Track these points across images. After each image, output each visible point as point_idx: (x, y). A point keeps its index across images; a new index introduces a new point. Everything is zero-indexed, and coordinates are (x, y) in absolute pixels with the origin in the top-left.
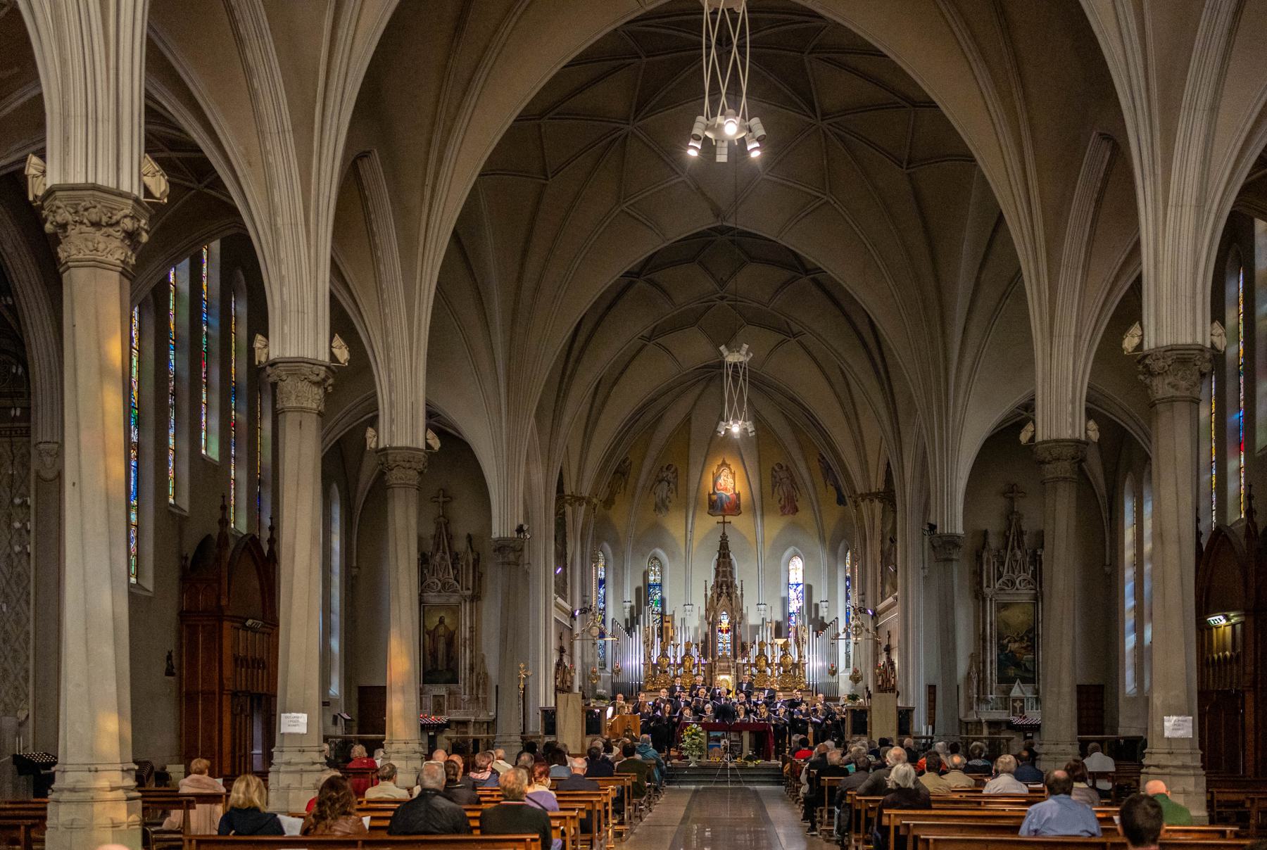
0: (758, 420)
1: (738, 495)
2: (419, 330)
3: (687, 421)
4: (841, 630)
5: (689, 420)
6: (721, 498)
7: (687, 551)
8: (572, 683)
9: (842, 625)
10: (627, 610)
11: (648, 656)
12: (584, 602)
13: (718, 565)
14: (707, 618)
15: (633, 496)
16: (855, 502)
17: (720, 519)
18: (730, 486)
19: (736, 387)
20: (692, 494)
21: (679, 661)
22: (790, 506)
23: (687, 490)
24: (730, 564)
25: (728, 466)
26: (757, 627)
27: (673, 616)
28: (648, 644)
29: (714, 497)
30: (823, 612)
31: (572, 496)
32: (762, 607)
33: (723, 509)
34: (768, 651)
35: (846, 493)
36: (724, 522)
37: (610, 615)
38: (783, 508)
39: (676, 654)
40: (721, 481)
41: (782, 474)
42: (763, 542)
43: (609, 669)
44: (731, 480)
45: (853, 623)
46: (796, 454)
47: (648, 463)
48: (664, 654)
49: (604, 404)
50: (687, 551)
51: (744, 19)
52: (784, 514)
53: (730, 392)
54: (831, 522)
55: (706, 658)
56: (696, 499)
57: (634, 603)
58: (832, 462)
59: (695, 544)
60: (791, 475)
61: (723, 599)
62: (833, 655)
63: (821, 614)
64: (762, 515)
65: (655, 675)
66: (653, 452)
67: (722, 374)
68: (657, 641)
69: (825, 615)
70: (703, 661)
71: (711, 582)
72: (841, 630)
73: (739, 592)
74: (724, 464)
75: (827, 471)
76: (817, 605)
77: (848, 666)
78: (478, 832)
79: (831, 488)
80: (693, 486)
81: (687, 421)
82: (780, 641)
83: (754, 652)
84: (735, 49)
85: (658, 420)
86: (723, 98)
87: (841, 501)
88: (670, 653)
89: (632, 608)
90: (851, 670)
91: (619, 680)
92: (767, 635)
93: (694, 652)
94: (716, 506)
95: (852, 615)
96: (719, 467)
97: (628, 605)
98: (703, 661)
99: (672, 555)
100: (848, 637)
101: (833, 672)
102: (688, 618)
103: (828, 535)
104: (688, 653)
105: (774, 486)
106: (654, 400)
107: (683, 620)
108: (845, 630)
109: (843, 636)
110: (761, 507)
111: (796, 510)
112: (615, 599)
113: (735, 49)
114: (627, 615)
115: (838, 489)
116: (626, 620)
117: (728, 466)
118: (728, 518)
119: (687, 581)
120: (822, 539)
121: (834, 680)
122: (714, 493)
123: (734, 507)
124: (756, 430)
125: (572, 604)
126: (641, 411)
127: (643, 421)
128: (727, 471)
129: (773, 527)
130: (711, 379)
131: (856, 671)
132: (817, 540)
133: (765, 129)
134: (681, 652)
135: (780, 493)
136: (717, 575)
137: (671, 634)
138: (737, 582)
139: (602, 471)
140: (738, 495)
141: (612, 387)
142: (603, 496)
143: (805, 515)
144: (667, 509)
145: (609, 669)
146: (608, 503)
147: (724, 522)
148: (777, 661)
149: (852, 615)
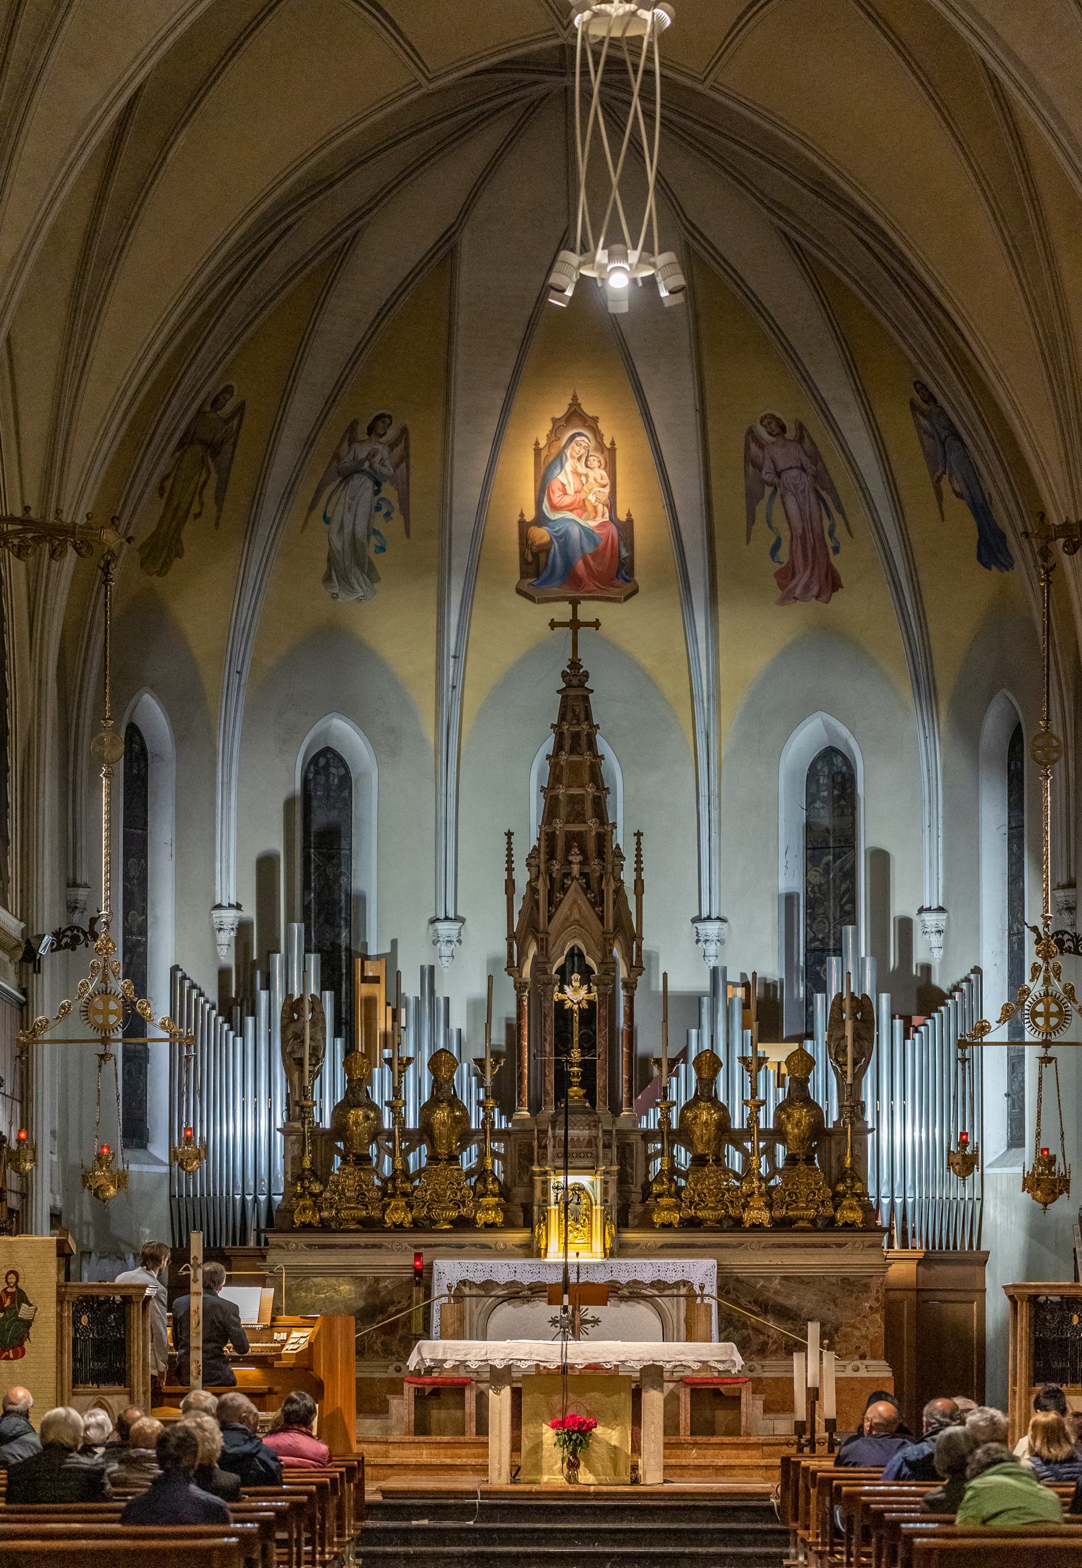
0: (698, 256)
1: (626, 529)
2: (236, 711)
3: (444, 255)
4: (991, 1011)
5: (453, 252)
6: (564, 538)
7: (445, 728)
8: (24, 1195)
9: (994, 997)
10: (227, 937)
11: (299, 1106)
12: (72, 907)
13: (556, 777)
14: (513, 967)
15: (250, 524)
16: (1045, 553)
17: (562, 611)
18: (597, 495)
19: (616, 124)
20: (462, 523)
21: (411, 1123)
22: (810, 573)
23: (445, 506)
24: (596, 776)
25: (591, 424)
26: (694, 1000)
27: (390, 959)
28: (300, 1063)
29: (541, 535)
30: (927, 948)
31: (26, 522)
32: (711, 929)
33: (571, 577)
34: (732, 1089)
35: (1006, 517)
36: (575, 624)
37: (165, 949)
38: (785, 576)
39: (403, 1094)
40: (565, 477)
41: (785, 455)
42: (715, 695)
43: (160, 1149)
44: (599, 474)
45: (1036, 988)
46: (834, 384)
47: (303, 406)
48: (355, 1095)
49: (143, 188)
50: (445, 728)
51: (650, 50)
52: (787, 598)
53: (596, 155)
54: (954, 628)
55: (508, 1110)
56: (477, 536)
57: (250, 912)
58: (961, 411)
59: (473, 700)
60: (816, 457)
61: (574, 902)
62: (965, 1098)
63: (920, 956)
64: (713, 599)
65: (321, 1173)
66: (319, 372)
67: (568, 91)
68: (334, 1049)
69: (936, 958)
70: (501, 1123)
71: (529, 838)
72: (991, 1011)
73: (628, 876)
74: (575, 415)
75: (944, 441)
76: (905, 925)
77: (1016, 1140)
78: (808, 1045)
79: (959, 510)
80: (466, 493)
81: (444, 255)
82: (777, 1053)
83: (682, 1087)
84: (636, 101)
85: (339, 252)
86: (616, 194)
87: (992, 550)
88: (380, 1091)
89: (243, 928)
90: (1028, 1152)
91: (196, 1188)
92: (728, 1036)
93: (468, 1089)
94: (547, 568)
95: (1031, 956)
96: (558, 426)
97: (229, 917)
98: (501, 1123)
99: (387, 742)
100: (1016, 1041)
101: (965, 1161)
102: (444, 968)
103: (945, 680)
104: (442, 1094)
105: (752, 499)
106: (321, 185)
107: (429, 975)
108: (1008, 1014)
109: (1000, 1033)
110: (709, 573)
111: (832, 583)
112: (181, 894)
113: (636, 101)
114: (227, 957)
115: (981, 511)
116: (223, 974)
117: (591, 424)
118: (588, 610)
119: (445, 829)
120: (926, 688)
121: (964, 1191)
122: (541, 519)
123: (613, 570)
124: (689, 291)
125: (24, 916)
126: (274, 223)
127: (286, 257)
128: (585, 441)
129: (753, 642)
130: (533, 107)
131: (1045, 1160)
132: (907, 692)
133: (685, 279)
134: (417, 1086)
135: (772, 525)
136: (550, 813)
137: (383, 1023)
138: (621, 838)
139: (137, 436)
140: (626, 529)
141: (173, 132)
142: (145, 526)
143: (865, 602)
144: (371, 574)
145: (160, 1149)
146: (162, 550)
147: (575, 624)
148: (766, 1120)
149: (1031, 956)
